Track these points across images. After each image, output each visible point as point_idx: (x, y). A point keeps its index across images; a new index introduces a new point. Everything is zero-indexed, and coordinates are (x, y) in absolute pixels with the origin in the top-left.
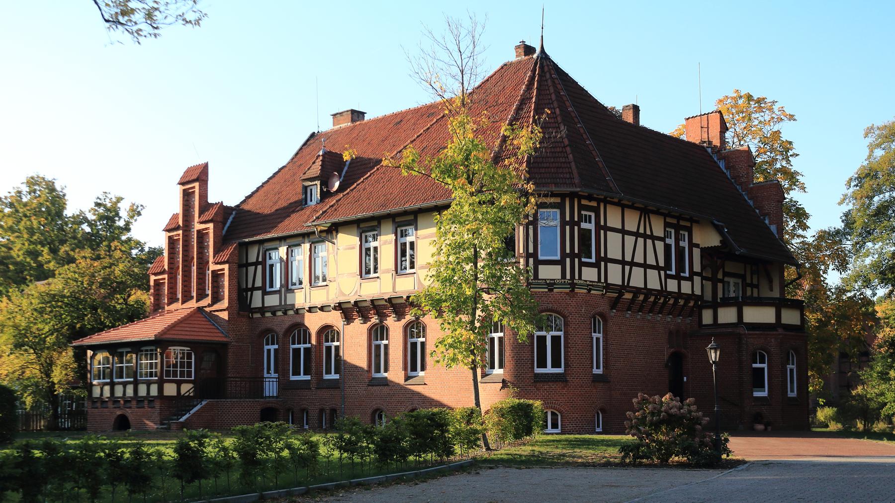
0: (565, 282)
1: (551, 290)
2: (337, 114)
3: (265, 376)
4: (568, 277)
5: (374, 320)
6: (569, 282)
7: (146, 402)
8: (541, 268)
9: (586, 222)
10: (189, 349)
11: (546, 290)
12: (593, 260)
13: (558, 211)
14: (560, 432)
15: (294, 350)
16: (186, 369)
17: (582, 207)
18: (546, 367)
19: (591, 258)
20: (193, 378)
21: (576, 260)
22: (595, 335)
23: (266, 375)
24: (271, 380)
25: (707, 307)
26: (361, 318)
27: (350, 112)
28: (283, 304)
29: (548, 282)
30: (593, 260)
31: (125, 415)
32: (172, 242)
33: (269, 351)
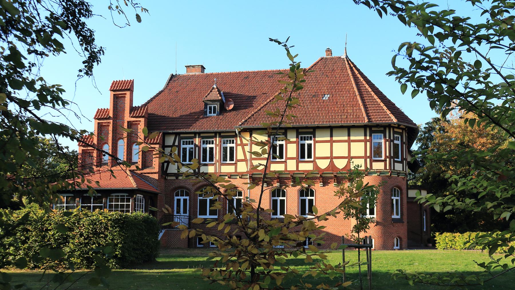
2: (191, 66)
5: (276, 185)
9: (396, 140)
10: (127, 194)
11: (397, 176)
12: (400, 160)
13: (383, 135)
14: (399, 248)
15: (177, 199)
16: (125, 209)
17: (395, 133)
18: (277, 215)
19: (398, 158)
21: (392, 160)
22: (394, 198)
23: (175, 214)
24: (182, 217)
27: (200, 66)
30: (400, 160)
32: (100, 127)
33: (179, 200)
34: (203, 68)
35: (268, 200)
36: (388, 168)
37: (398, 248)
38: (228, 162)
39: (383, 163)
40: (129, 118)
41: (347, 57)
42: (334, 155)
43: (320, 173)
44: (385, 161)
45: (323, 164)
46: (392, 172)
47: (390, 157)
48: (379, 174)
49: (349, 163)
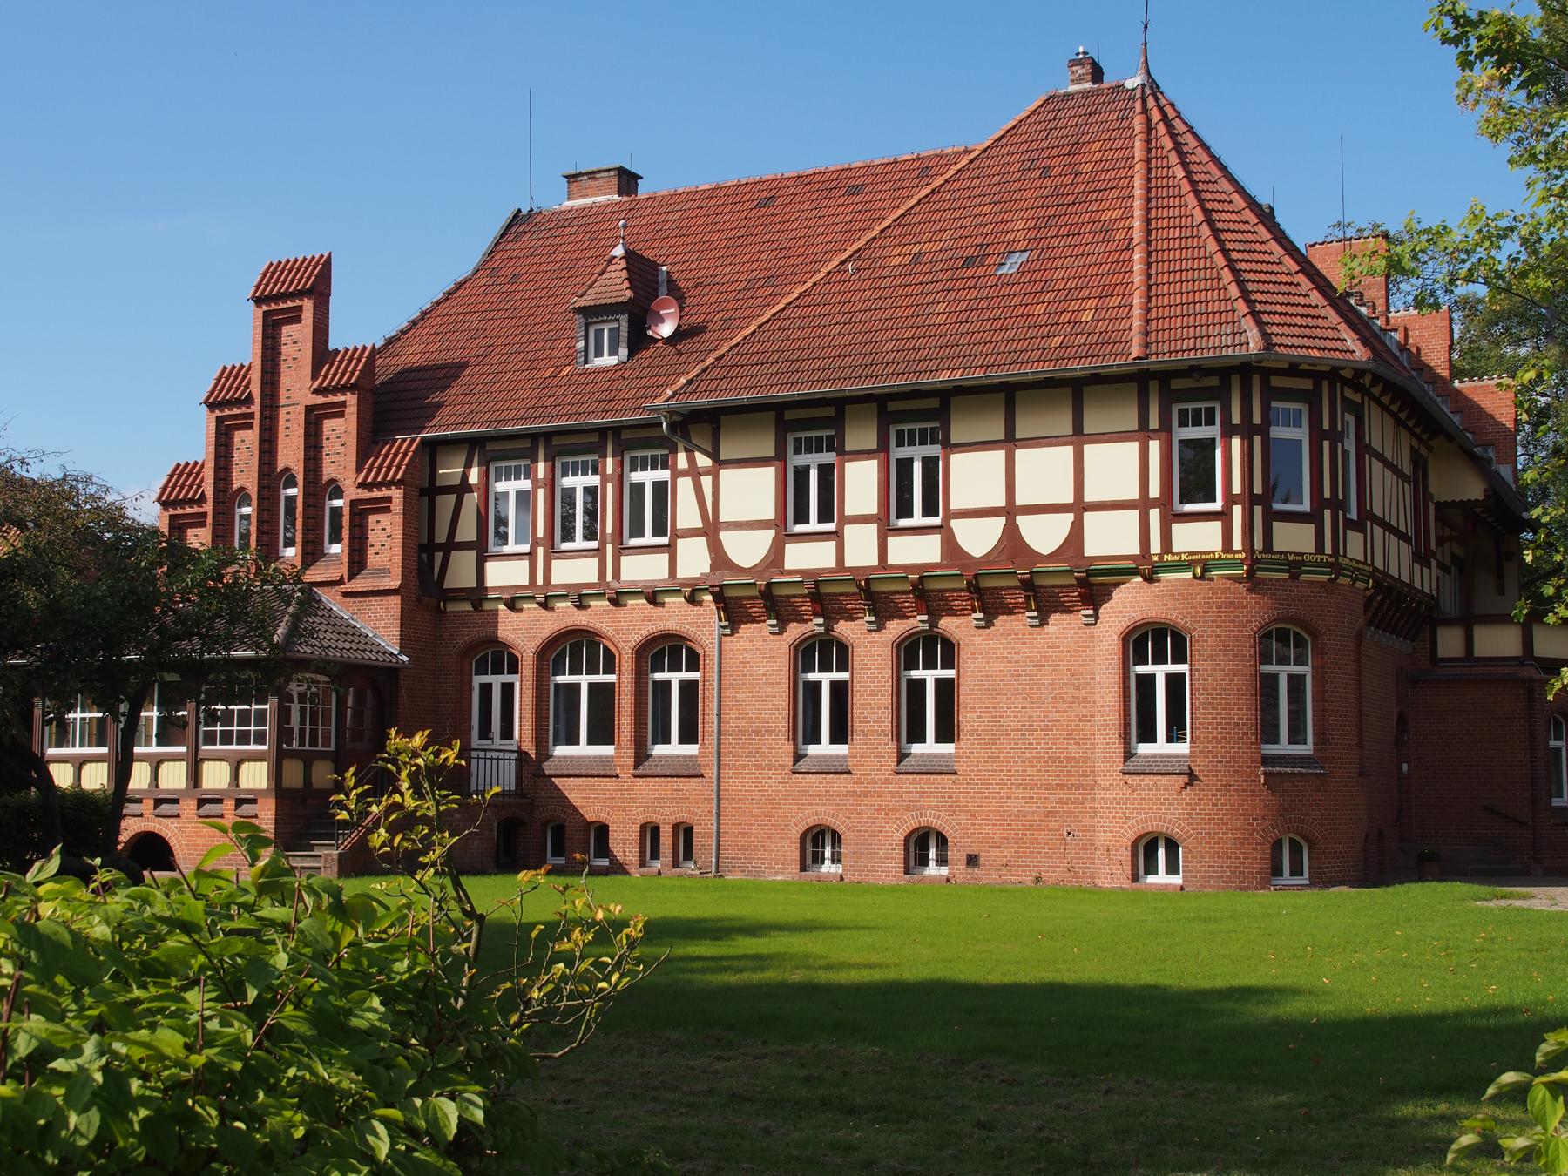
0: (1322, 559)
1: (1294, 577)
3: (474, 746)
4: (1328, 549)
6: (1330, 560)
7: (150, 803)
8: (1177, 529)
11: (1286, 576)
12: (1306, 507)
17: (1269, 394)
20: (332, 748)
24: (495, 755)
25: (1449, 622)
26: (774, 622)
28: (540, 581)
29: (1291, 558)
31: (154, 833)
34: (627, 180)
35: (784, 686)
36: (1237, 545)
37: (1304, 880)
38: (579, 543)
39: (1216, 527)
40: (310, 395)
41: (1152, 87)
42: (1020, 500)
43: (970, 574)
44: (1224, 516)
45: (978, 539)
46: (1258, 561)
47: (1249, 500)
48: (1199, 571)
49: (1077, 530)
